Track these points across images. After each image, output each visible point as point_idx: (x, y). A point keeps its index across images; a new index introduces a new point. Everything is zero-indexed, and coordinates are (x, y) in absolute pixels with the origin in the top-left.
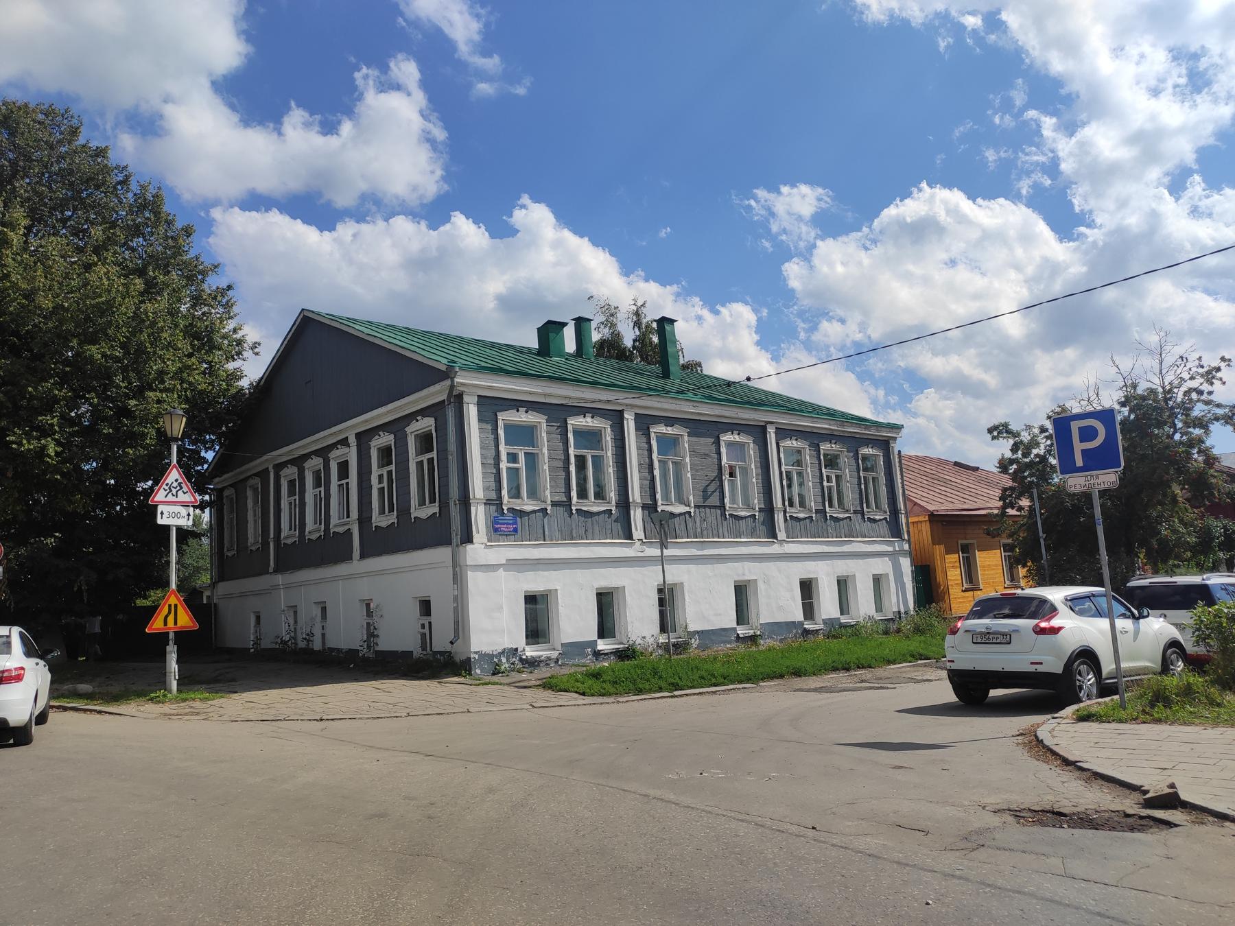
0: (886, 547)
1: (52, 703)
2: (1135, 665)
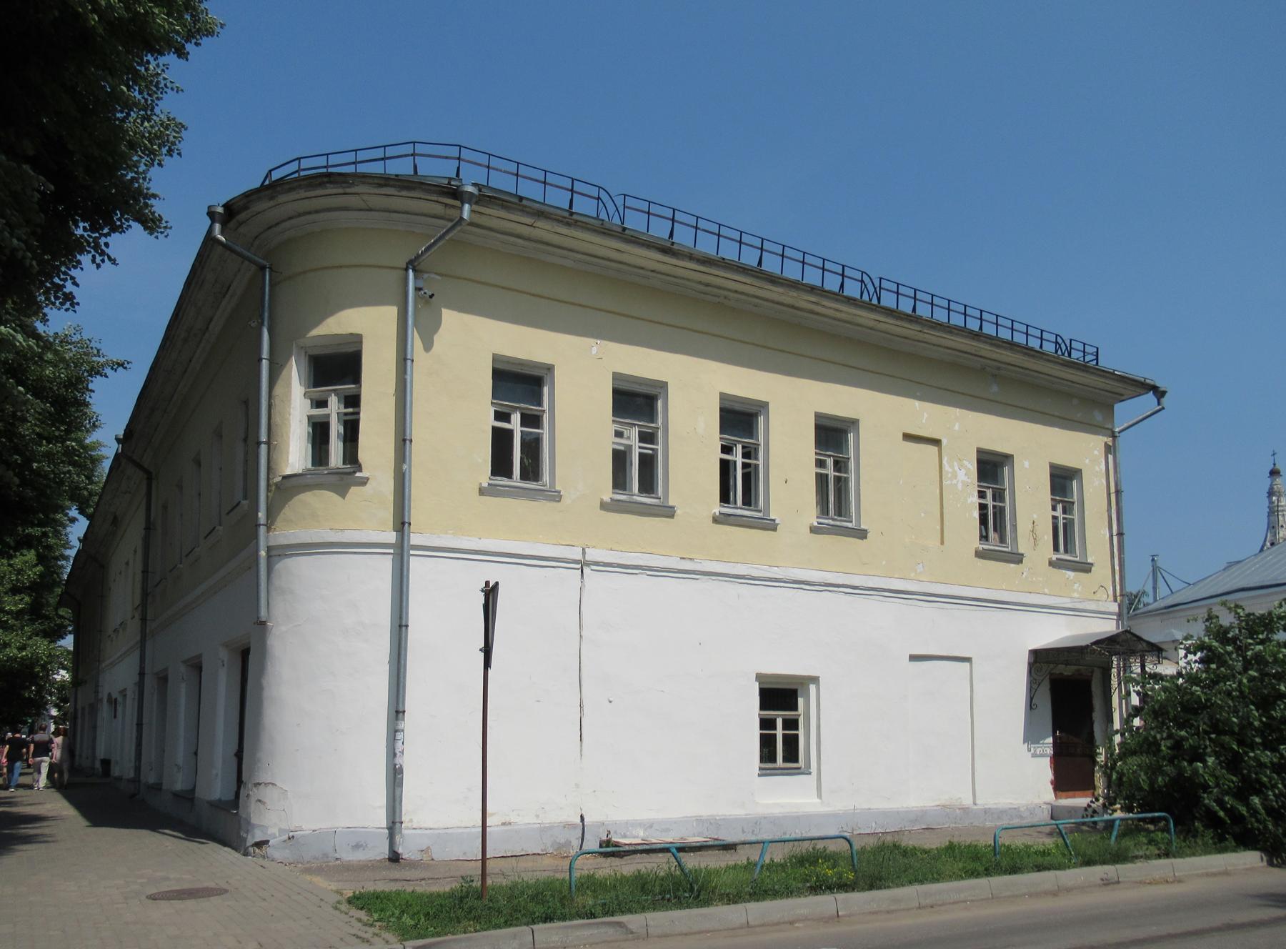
0: (293, 380)
1: (980, 484)
2: (659, 475)
